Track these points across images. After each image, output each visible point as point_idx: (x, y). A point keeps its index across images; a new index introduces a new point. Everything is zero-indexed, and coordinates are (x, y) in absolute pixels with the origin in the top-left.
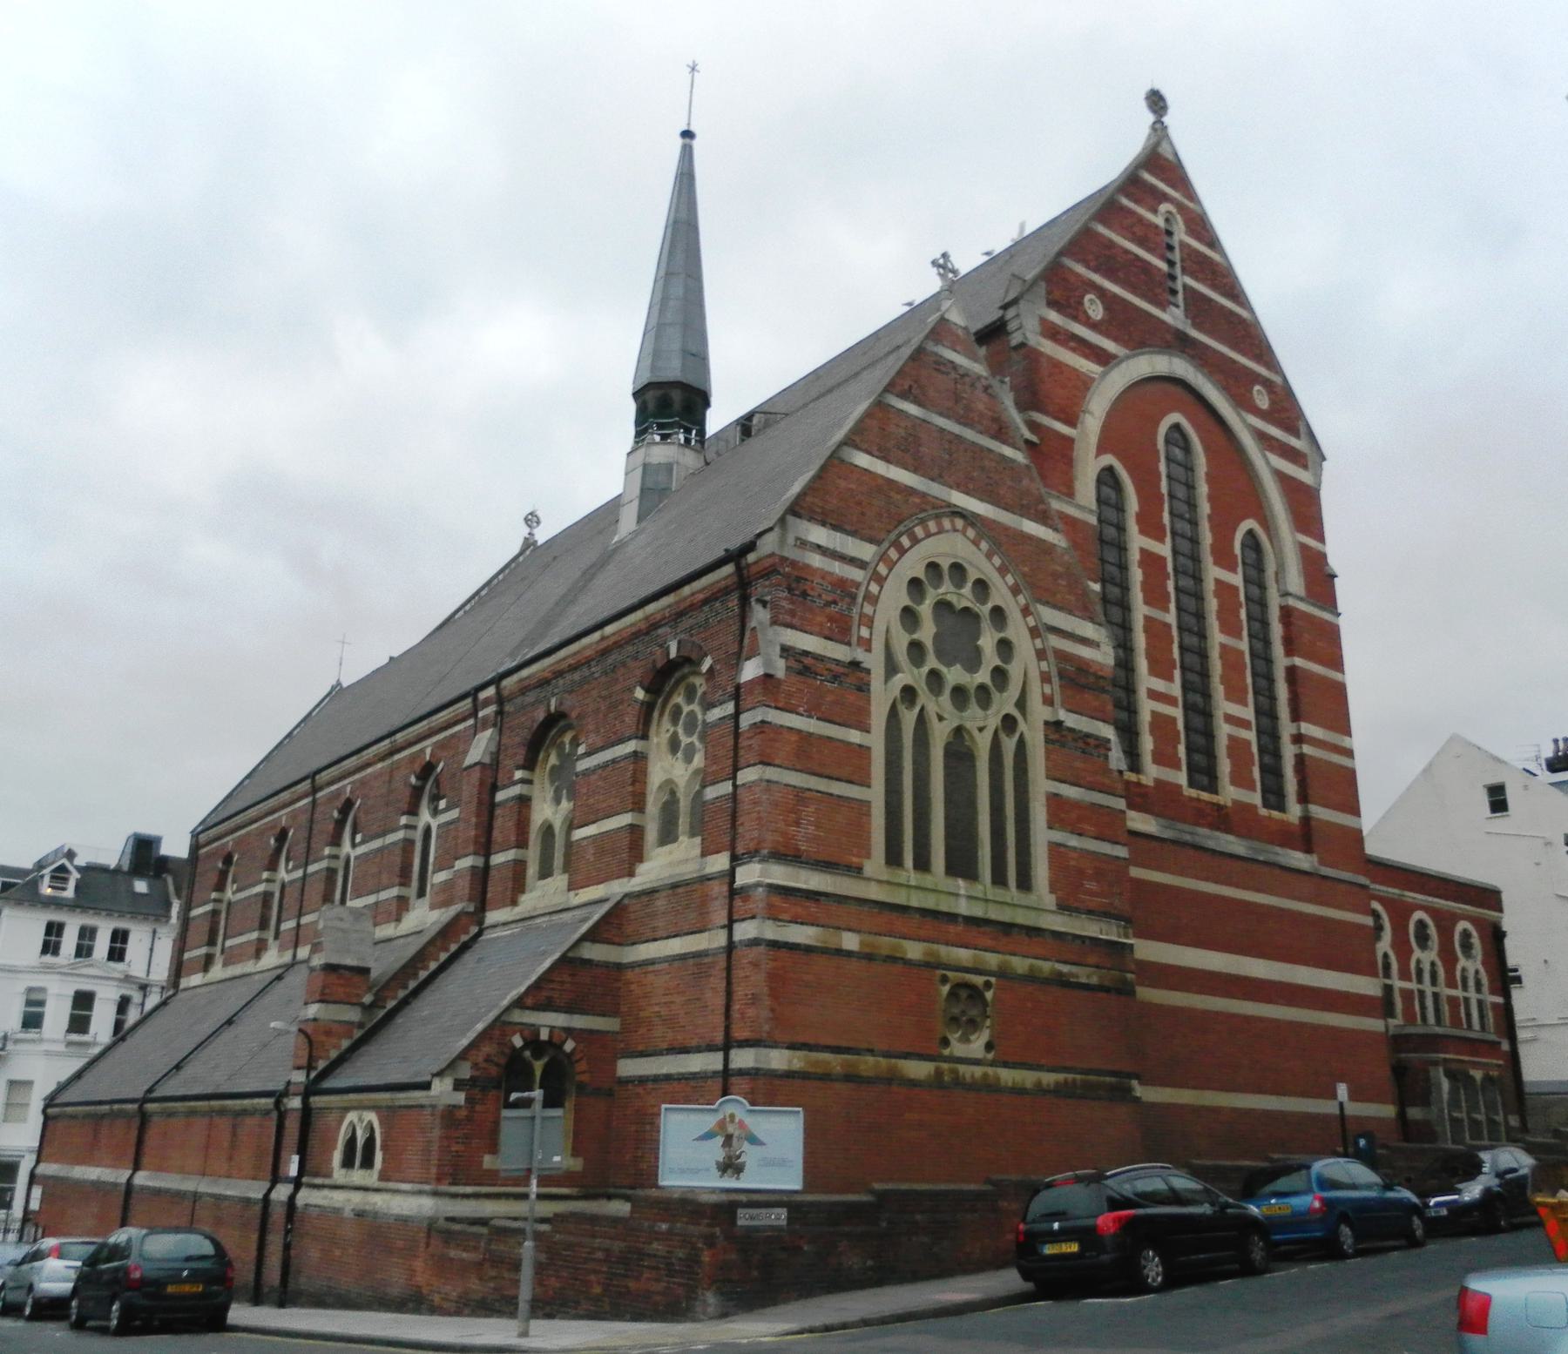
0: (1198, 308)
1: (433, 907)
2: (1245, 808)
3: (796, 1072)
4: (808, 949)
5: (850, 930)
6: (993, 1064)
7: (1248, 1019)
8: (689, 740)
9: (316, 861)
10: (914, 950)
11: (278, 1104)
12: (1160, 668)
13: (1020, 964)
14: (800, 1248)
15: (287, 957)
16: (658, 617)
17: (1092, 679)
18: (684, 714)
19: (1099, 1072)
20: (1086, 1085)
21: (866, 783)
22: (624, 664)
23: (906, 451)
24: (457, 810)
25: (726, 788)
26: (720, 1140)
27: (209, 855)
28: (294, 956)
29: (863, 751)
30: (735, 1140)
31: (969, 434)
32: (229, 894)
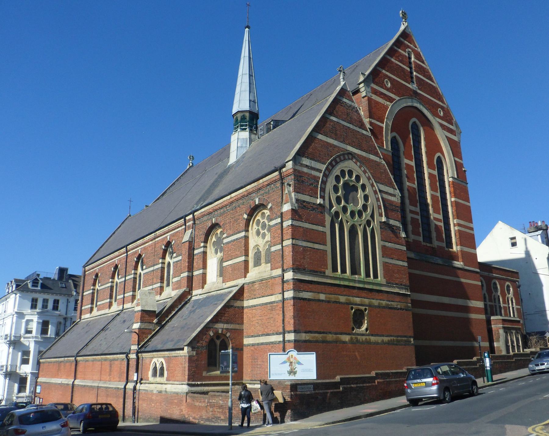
0: (420, 83)
1: (173, 290)
2: (440, 248)
3: (307, 340)
4: (309, 300)
5: (322, 293)
6: (368, 335)
8: (263, 232)
9: (129, 275)
10: (342, 299)
11: (127, 356)
12: (413, 203)
13: (375, 302)
14: (318, 398)
16: (251, 190)
17: (394, 207)
20: (397, 341)
22: (239, 206)
23: (333, 133)
24: (181, 257)
25: (279, 247)
26: (288, 364)
28: (123, 307)
30: (293, 364)
31: (351, 126)
32: (97, 287)
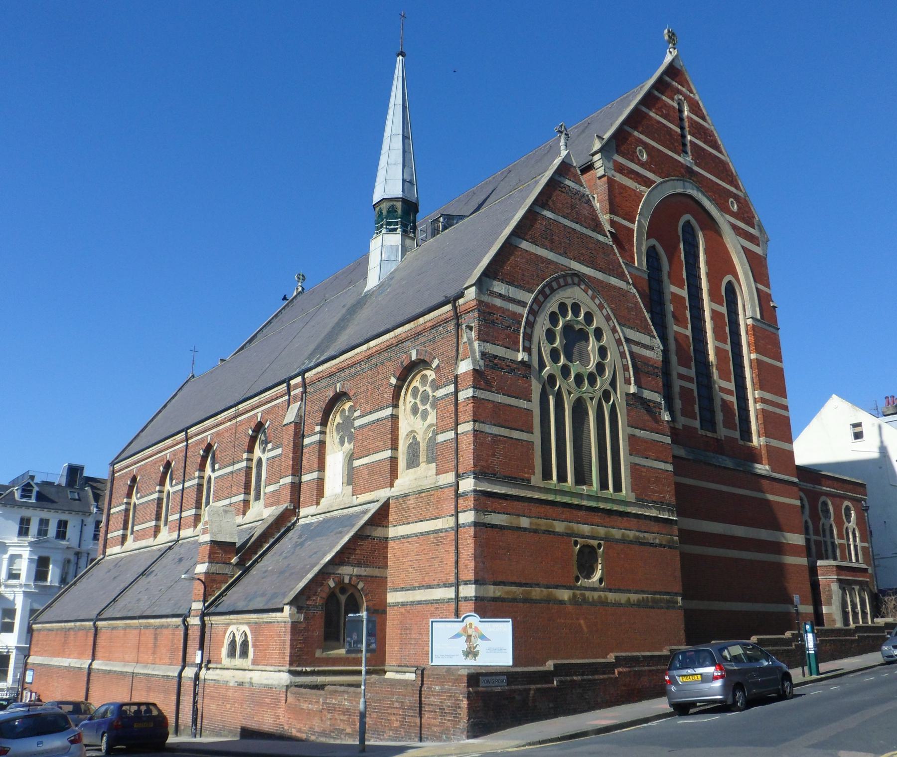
0: (700, 155)
1: (266, 506)
4: (502, 527)
5: (524, 516)
6: (603, 590)
7: (736, 560)
8: (424, 408)
9: (189, 480)
10: (559, 527)
13: (617, 533)
15: (174, 536)
16: (404, 336)
18: (421, 392)
19: (660, 593)
20: (654, 600)
21: (530, 431)
22: (382, 363)
25: (451, 435)
26: (464, 638)
27: (121, 477)
28: (179, 536)
29: (529, 412)
30: (473, 638)
31: (578, 227)
32: (134, 499)
